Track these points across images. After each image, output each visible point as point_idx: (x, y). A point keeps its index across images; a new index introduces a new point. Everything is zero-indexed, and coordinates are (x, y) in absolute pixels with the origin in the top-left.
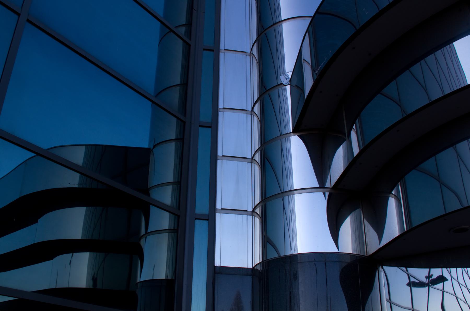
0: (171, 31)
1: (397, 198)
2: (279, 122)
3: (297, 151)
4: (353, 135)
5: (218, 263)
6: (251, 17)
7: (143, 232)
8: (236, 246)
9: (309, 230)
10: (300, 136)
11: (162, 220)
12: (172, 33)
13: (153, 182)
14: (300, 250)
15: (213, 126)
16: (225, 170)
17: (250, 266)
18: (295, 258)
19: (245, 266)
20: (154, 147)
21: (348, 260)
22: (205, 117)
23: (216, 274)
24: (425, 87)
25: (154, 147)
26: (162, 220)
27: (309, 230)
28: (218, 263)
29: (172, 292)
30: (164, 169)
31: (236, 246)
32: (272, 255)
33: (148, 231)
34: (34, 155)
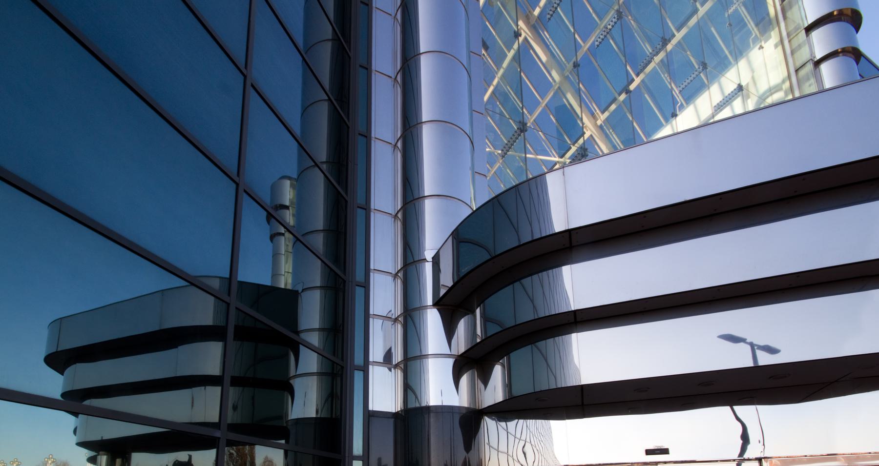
0: (316, 165)
1: (503, 366)
2: (421, 293)
3: (433, 320)
4: (478, 311)
5: (370, 408)
6: (395, 171)
7: (292, 372)
8: (384, 393)
9: (441, 389)
10: (438, 310)
11: (310, 361)
12: (317, 169)
13: (302, 326)
14: (432, 403)
15: (366, 286)
16: (376, 326)
17: (394, 411)
18: (428, 408)
19: (390, 411)
20: (303, 290)
21: (464, 411)
22: (359, 276)
23: (370, 416)
24: (531, 295)
25: (303, 290)
26: (310, 361)
27: (441, 389)
28: (370, 408)
29: (331, 429)
30: (312, 314)
31: (384, 393)
32: (412, 404)
33: (746, 456)
34: (187, 284)
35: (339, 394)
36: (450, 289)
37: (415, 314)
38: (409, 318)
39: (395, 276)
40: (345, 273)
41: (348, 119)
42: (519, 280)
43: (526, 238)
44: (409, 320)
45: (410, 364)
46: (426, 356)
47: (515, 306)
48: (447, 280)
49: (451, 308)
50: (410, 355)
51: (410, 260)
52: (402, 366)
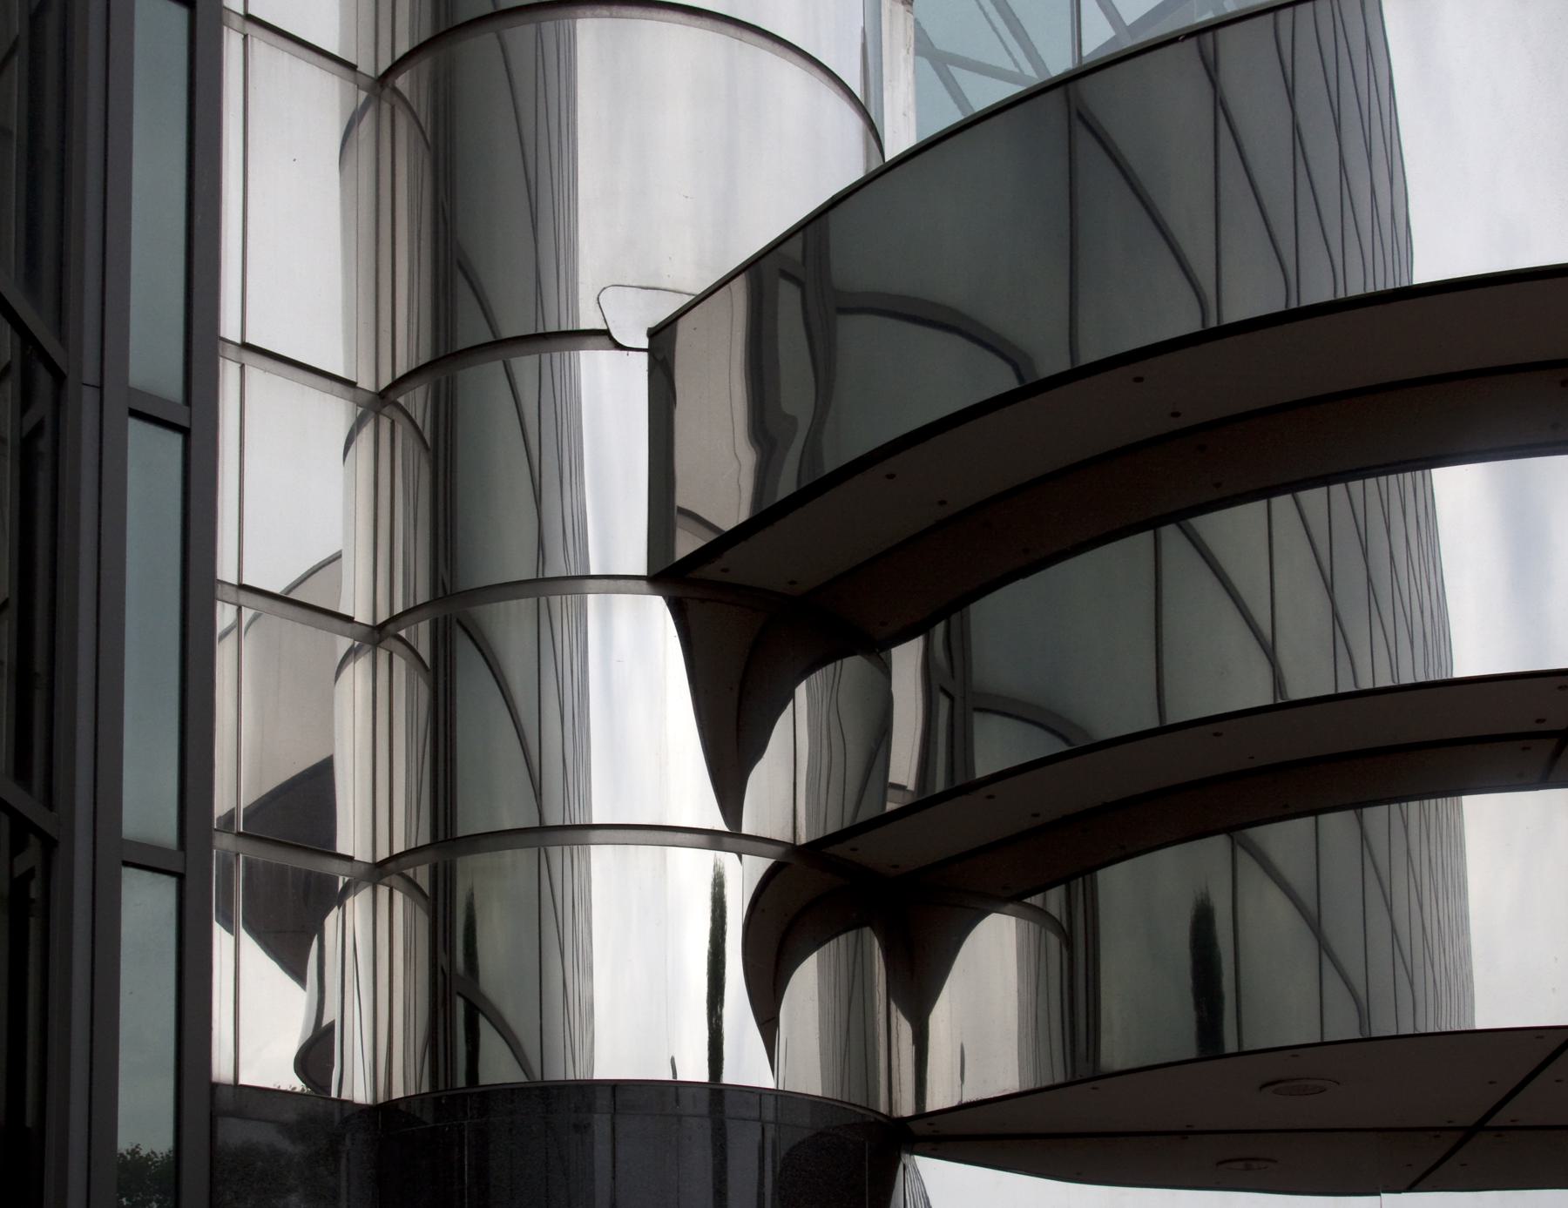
3: (635, 689)
5: (221, 1069)
15: (192, 425)
35: (90, 376)
36: (726, 541)
37: (510, 625)
38: (460, 623)
39: (377, 404)
40: (49, 801)
41: (62, 338)
42: (1358, 805)
43: (1251, 296)
44: (464, 650)
45: (481, 857)
46: (584, 832)
47: (1216, 619)
48: (722, 489)
49: (754, 623)
50: (468, 824)
51: (472, 331)
52: (422, 876)
